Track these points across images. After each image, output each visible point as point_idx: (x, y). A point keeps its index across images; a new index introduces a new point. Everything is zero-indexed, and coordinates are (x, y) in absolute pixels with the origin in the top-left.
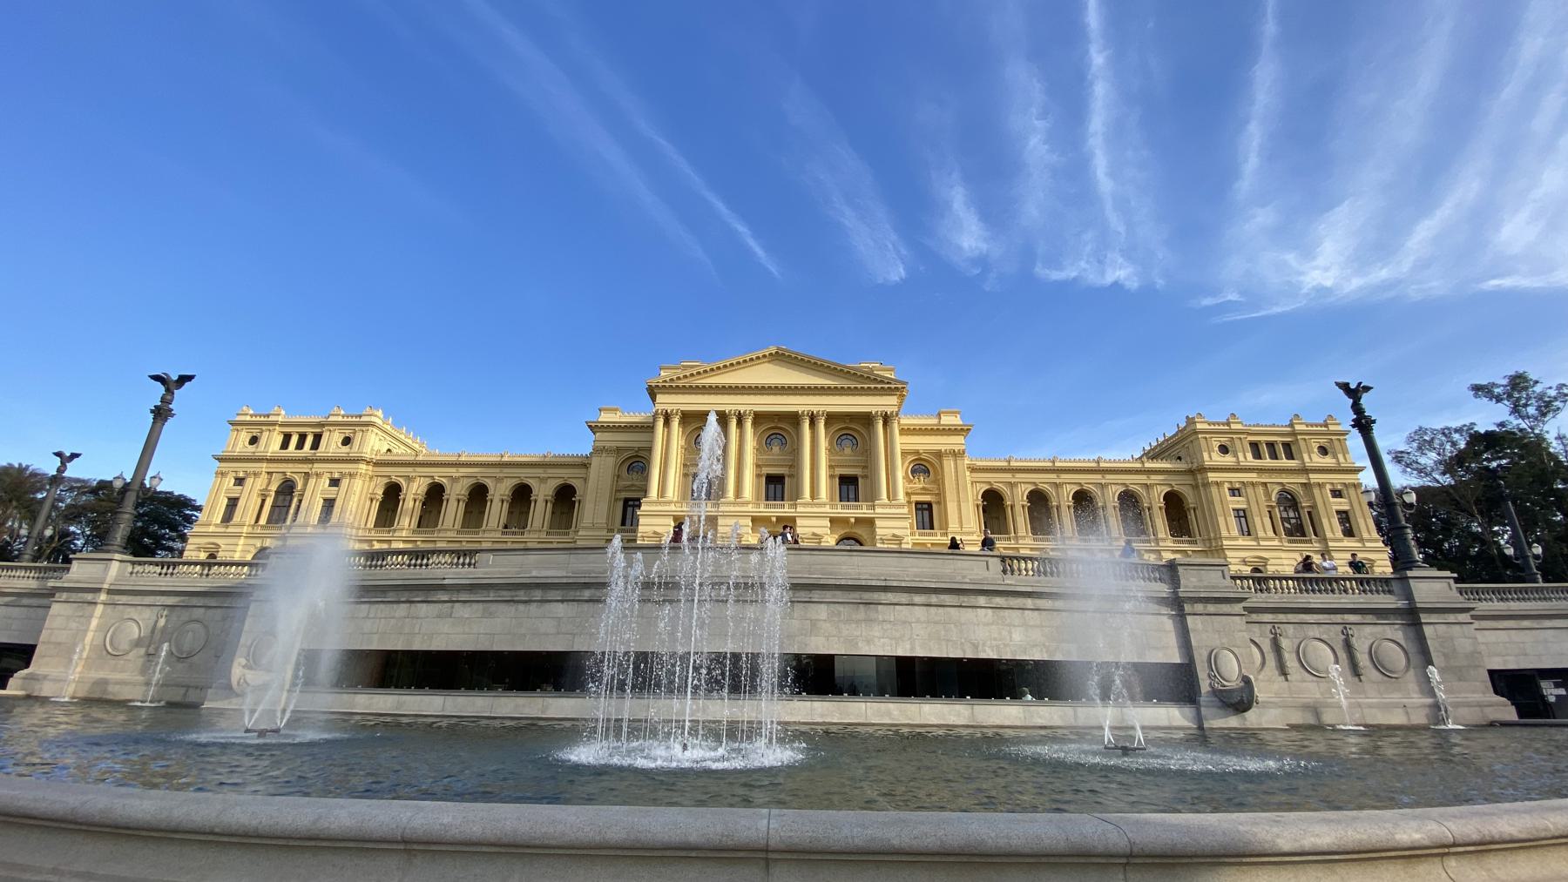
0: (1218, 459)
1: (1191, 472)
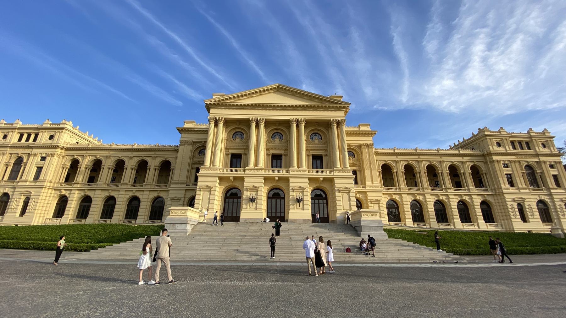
0: (496, 149)
1: (483, 156)
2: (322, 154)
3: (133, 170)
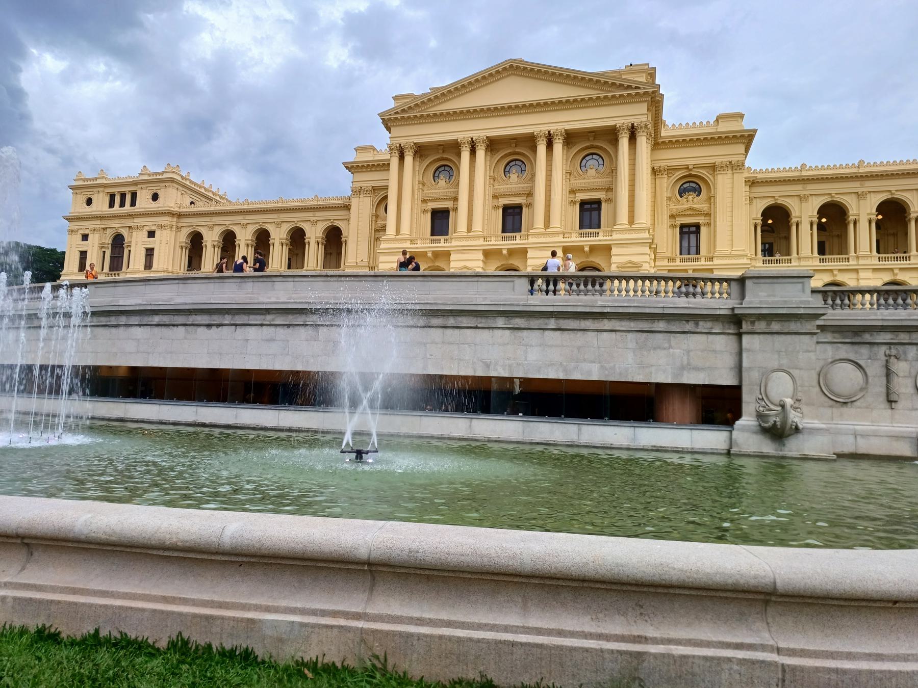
2: (448, 208)
3: (250, 247)
